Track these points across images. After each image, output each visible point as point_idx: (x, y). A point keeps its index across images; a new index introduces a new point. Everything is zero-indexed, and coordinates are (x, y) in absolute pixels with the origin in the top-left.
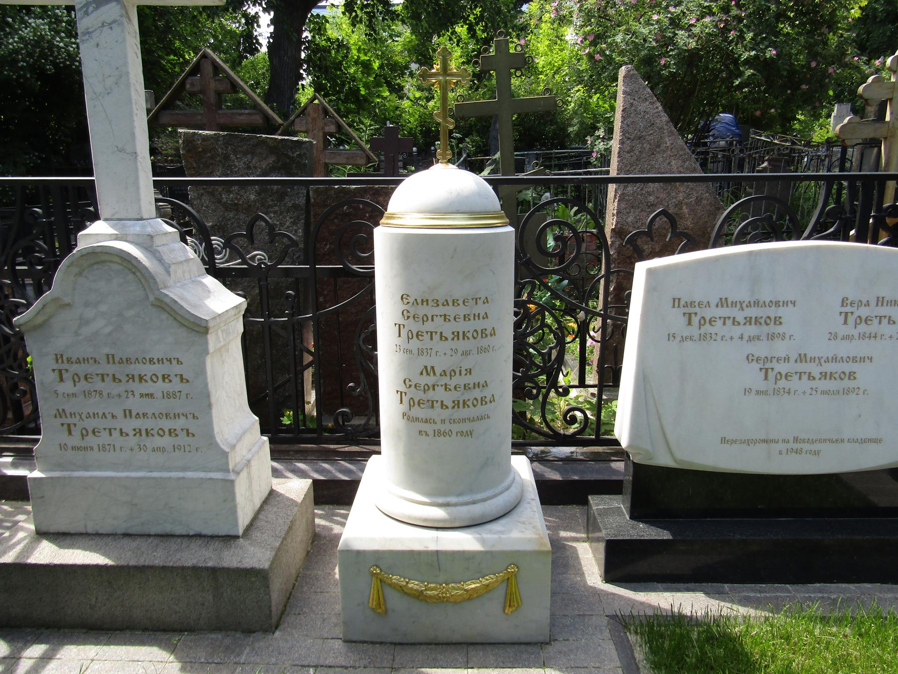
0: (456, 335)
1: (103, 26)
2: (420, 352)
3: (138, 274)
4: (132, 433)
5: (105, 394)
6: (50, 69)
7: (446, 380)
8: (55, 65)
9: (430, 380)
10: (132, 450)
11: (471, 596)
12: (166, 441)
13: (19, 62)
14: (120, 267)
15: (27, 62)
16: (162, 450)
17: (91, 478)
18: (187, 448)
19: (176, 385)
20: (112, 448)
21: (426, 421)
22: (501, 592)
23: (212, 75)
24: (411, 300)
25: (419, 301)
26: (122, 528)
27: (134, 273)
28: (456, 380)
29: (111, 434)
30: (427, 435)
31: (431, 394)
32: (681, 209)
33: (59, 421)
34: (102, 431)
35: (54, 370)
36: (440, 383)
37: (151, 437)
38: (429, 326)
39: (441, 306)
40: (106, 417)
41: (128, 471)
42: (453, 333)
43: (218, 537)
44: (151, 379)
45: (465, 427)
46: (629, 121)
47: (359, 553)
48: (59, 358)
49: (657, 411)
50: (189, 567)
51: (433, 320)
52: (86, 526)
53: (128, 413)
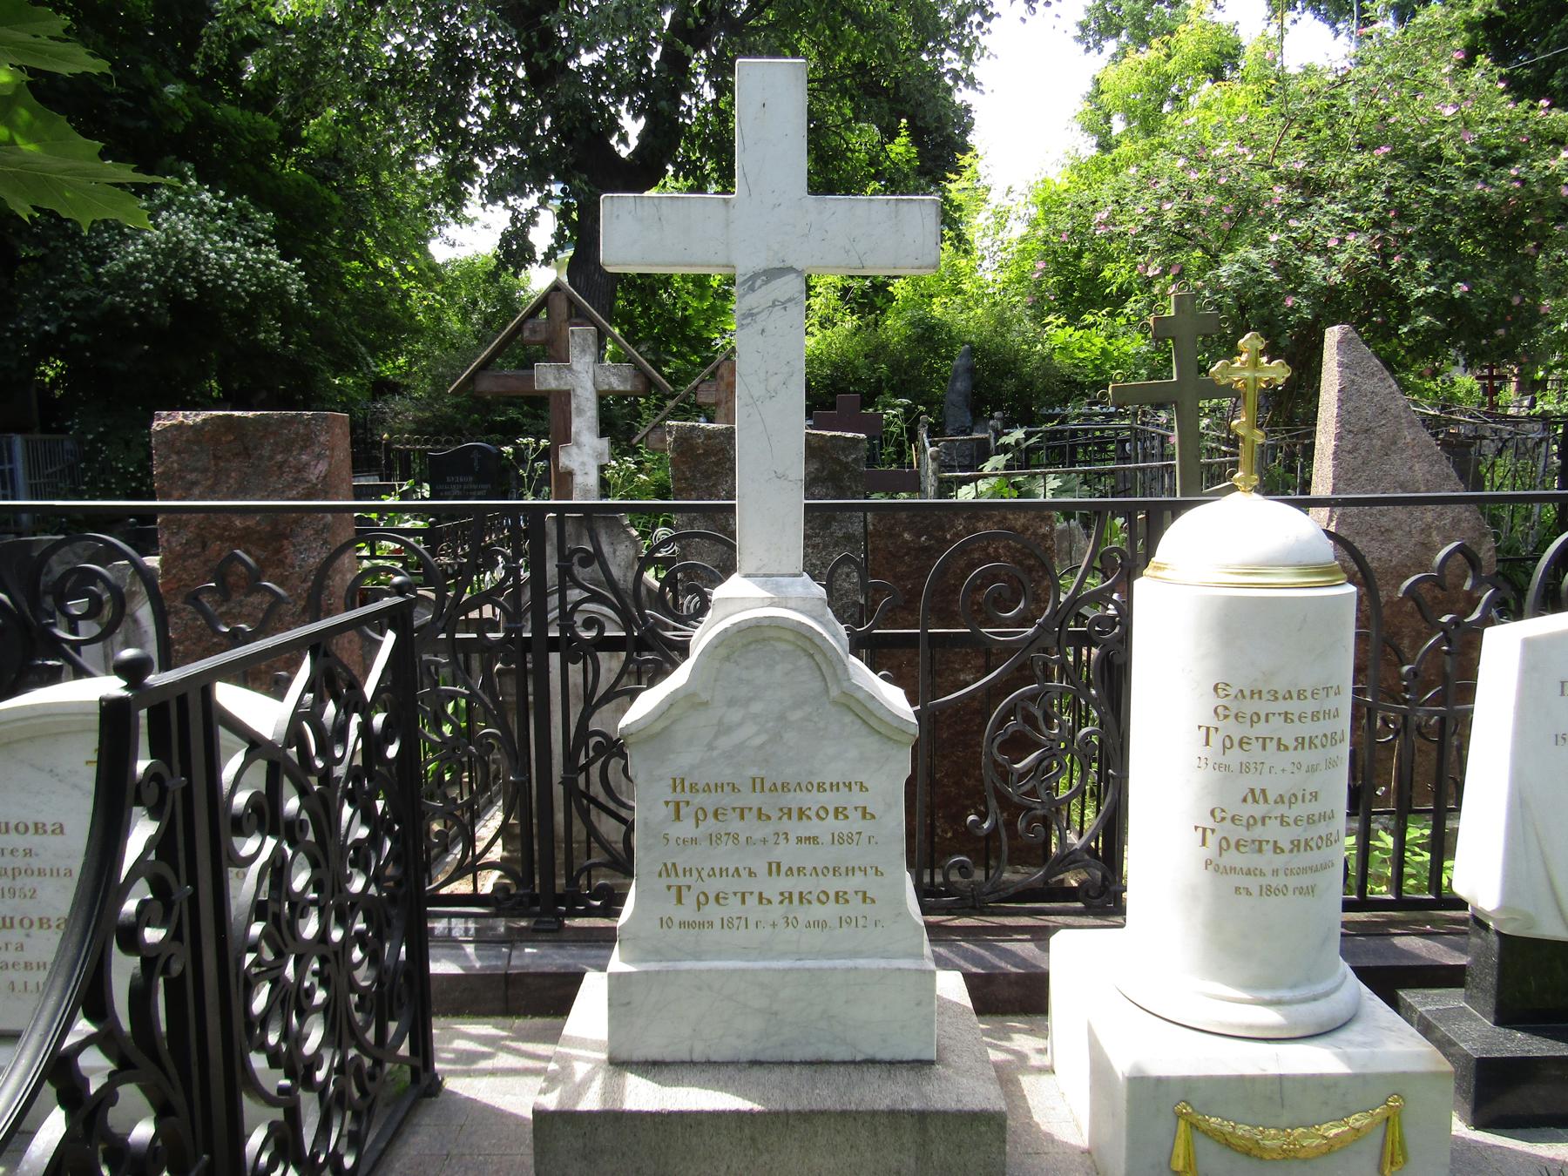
0: (1301, 742)
1: (774, 305)
2: (1244, 768)
3: (818, 657)
4: (776, 899)
5: (742, 839)
6: (191, 292)
7: (1282, 809)
8: (199, 284)
9: (1258, 810)
10: (774, 925)
11: (1331, 1148)
12: (830, 911)
13: (142, 282)
14: (790, 647)
15: (156, 283)
16: (821, 924)
17: (709, 971)
18: (861, 922)
19: (855, 823)
20: (743, 922)
21: (1249, 873)
22: (1372, 1144)
23: (565, 316)
24: (1233, 691)
25: (1247, 693)
26: (747, 1050)
27: (811, 656)
28: (1299, 810)
29: (743, 902)
30: (1249, 893)
31: (1258, 832)
32: (1430, 535)
33: (665, 881)
34: (731, 896)
35: (667, 803)
36: (1273, 815)
37: (806, 905)
38: (1261, 729)
39: (1281, 700)
40: (739, 875)
41: (764, 959)
42: (1296, 740)
43: (901, 1062)
44: (818, 815)
45: (1305, 880)
46: (1350, 406)
47: (1159, 1081)
48: (677, 784)
49: (1542, 853)
50: (883, 1112)
51: (1267, 721)
52: (691, 1052)
53: (774, 868)
